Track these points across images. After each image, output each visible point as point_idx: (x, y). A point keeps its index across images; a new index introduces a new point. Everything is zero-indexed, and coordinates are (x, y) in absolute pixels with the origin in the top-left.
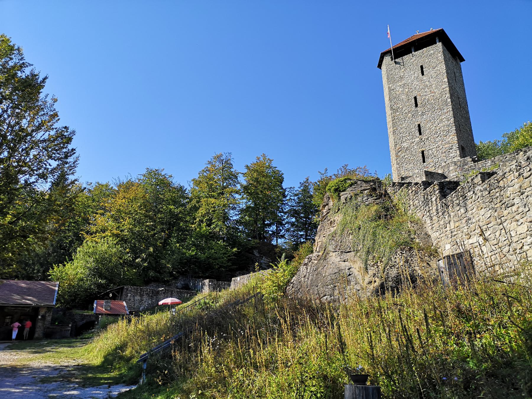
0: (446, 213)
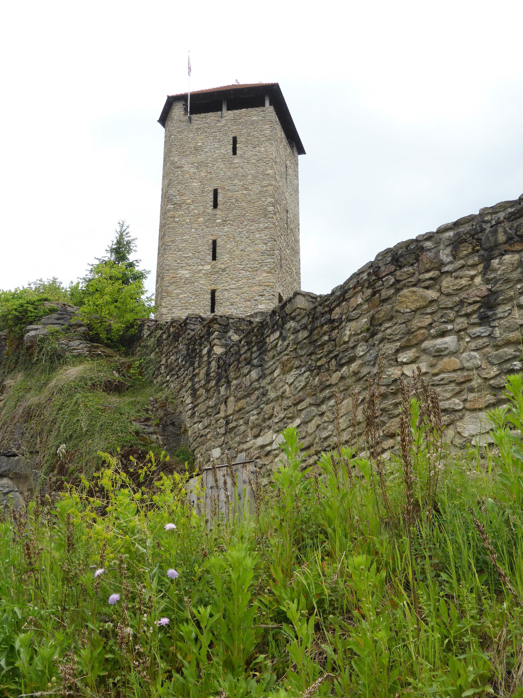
0: (223, 380)
